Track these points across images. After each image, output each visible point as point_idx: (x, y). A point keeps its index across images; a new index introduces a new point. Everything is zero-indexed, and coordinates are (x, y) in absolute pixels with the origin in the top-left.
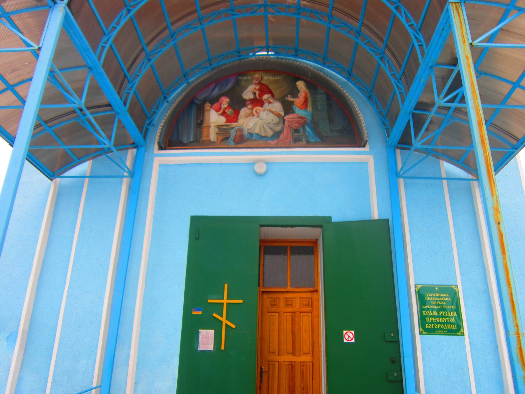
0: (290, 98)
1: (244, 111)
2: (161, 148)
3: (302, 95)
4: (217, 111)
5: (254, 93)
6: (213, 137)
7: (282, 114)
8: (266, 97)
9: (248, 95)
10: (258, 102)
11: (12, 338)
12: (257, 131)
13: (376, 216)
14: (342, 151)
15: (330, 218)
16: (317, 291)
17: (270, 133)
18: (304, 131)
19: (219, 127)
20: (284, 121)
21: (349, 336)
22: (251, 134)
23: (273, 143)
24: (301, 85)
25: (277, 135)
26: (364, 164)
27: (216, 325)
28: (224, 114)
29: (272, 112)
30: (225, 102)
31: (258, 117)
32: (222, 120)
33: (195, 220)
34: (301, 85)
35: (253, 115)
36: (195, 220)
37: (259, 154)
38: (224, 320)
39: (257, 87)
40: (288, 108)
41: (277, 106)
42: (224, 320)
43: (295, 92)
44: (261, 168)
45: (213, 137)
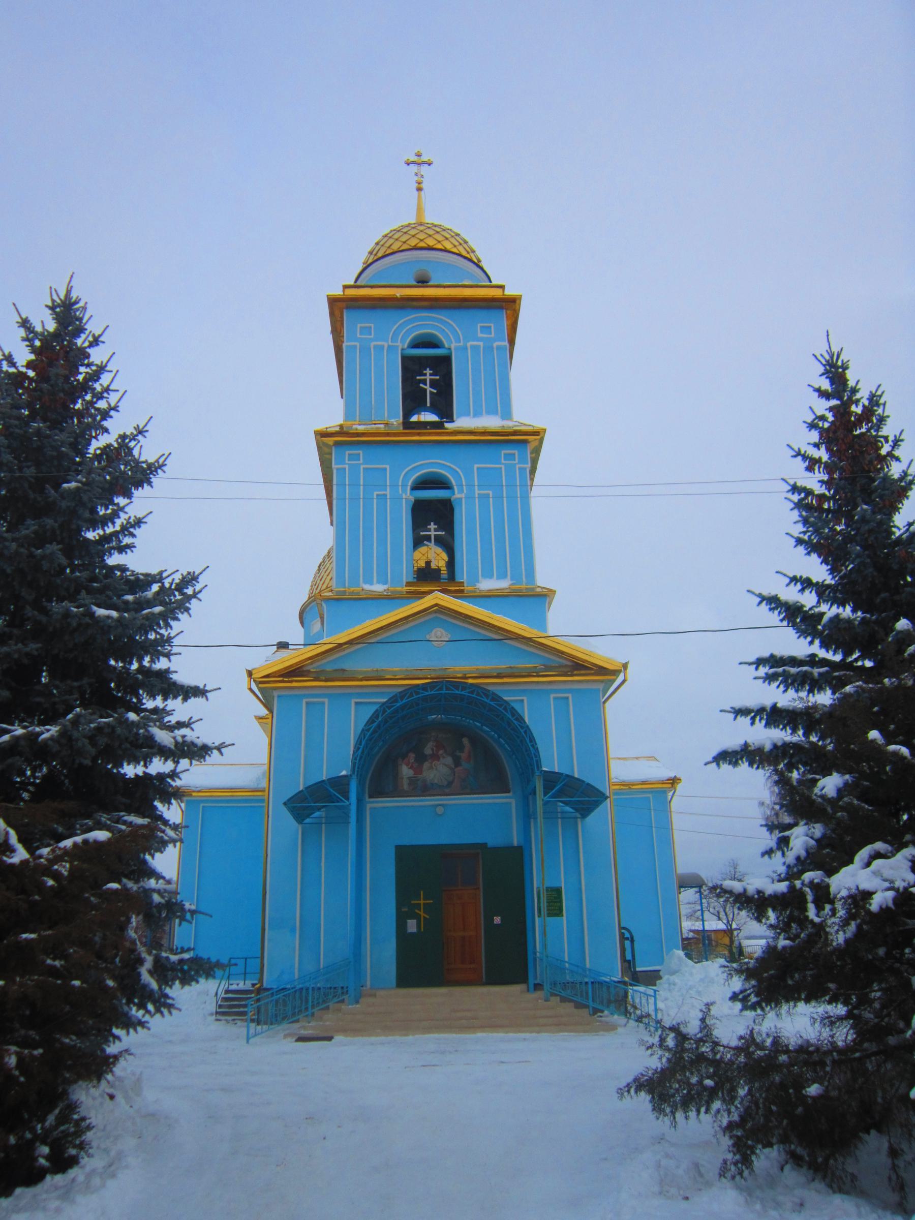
0: (458, 754)
1: (426, 765)
2: (370, 797)
3: (466, 750)
4: (407, 765)
5: (432, 750)
6: (406, 787)
7: (453, 766)
8: (441, 752)
9: (428, 751)
10: (435, 757)
11: (293, 930)
12: (436, 781)
13: (515, 843)
14: (897, 509)
15: (484, 845)
16: (478, 888)
17: (445, 783)
18: (753, 1035)
19: (409, 778)
20: (454, 773)
21: (497, 920)
22: (432, 784)
23: (447, 791)
24: (465, 741)
25: (450, 784)
26: (510, 803)
27: (417, 917)
28: (411, 768)
29: (446, 765)
30: (412, 756)
31: (436, 769)
32: (411, 773)
33: (398, 848)
34: (465, 741)
35: (433, 768)
36: (398, 848)
37: (481, 798)
38: (422, 913)
39: (434, 744)
40: (457, 762)
41: (449, 760)
42: (422, 913)
43: (461, 748)
44: (440, 810)
45: (406, 787)
